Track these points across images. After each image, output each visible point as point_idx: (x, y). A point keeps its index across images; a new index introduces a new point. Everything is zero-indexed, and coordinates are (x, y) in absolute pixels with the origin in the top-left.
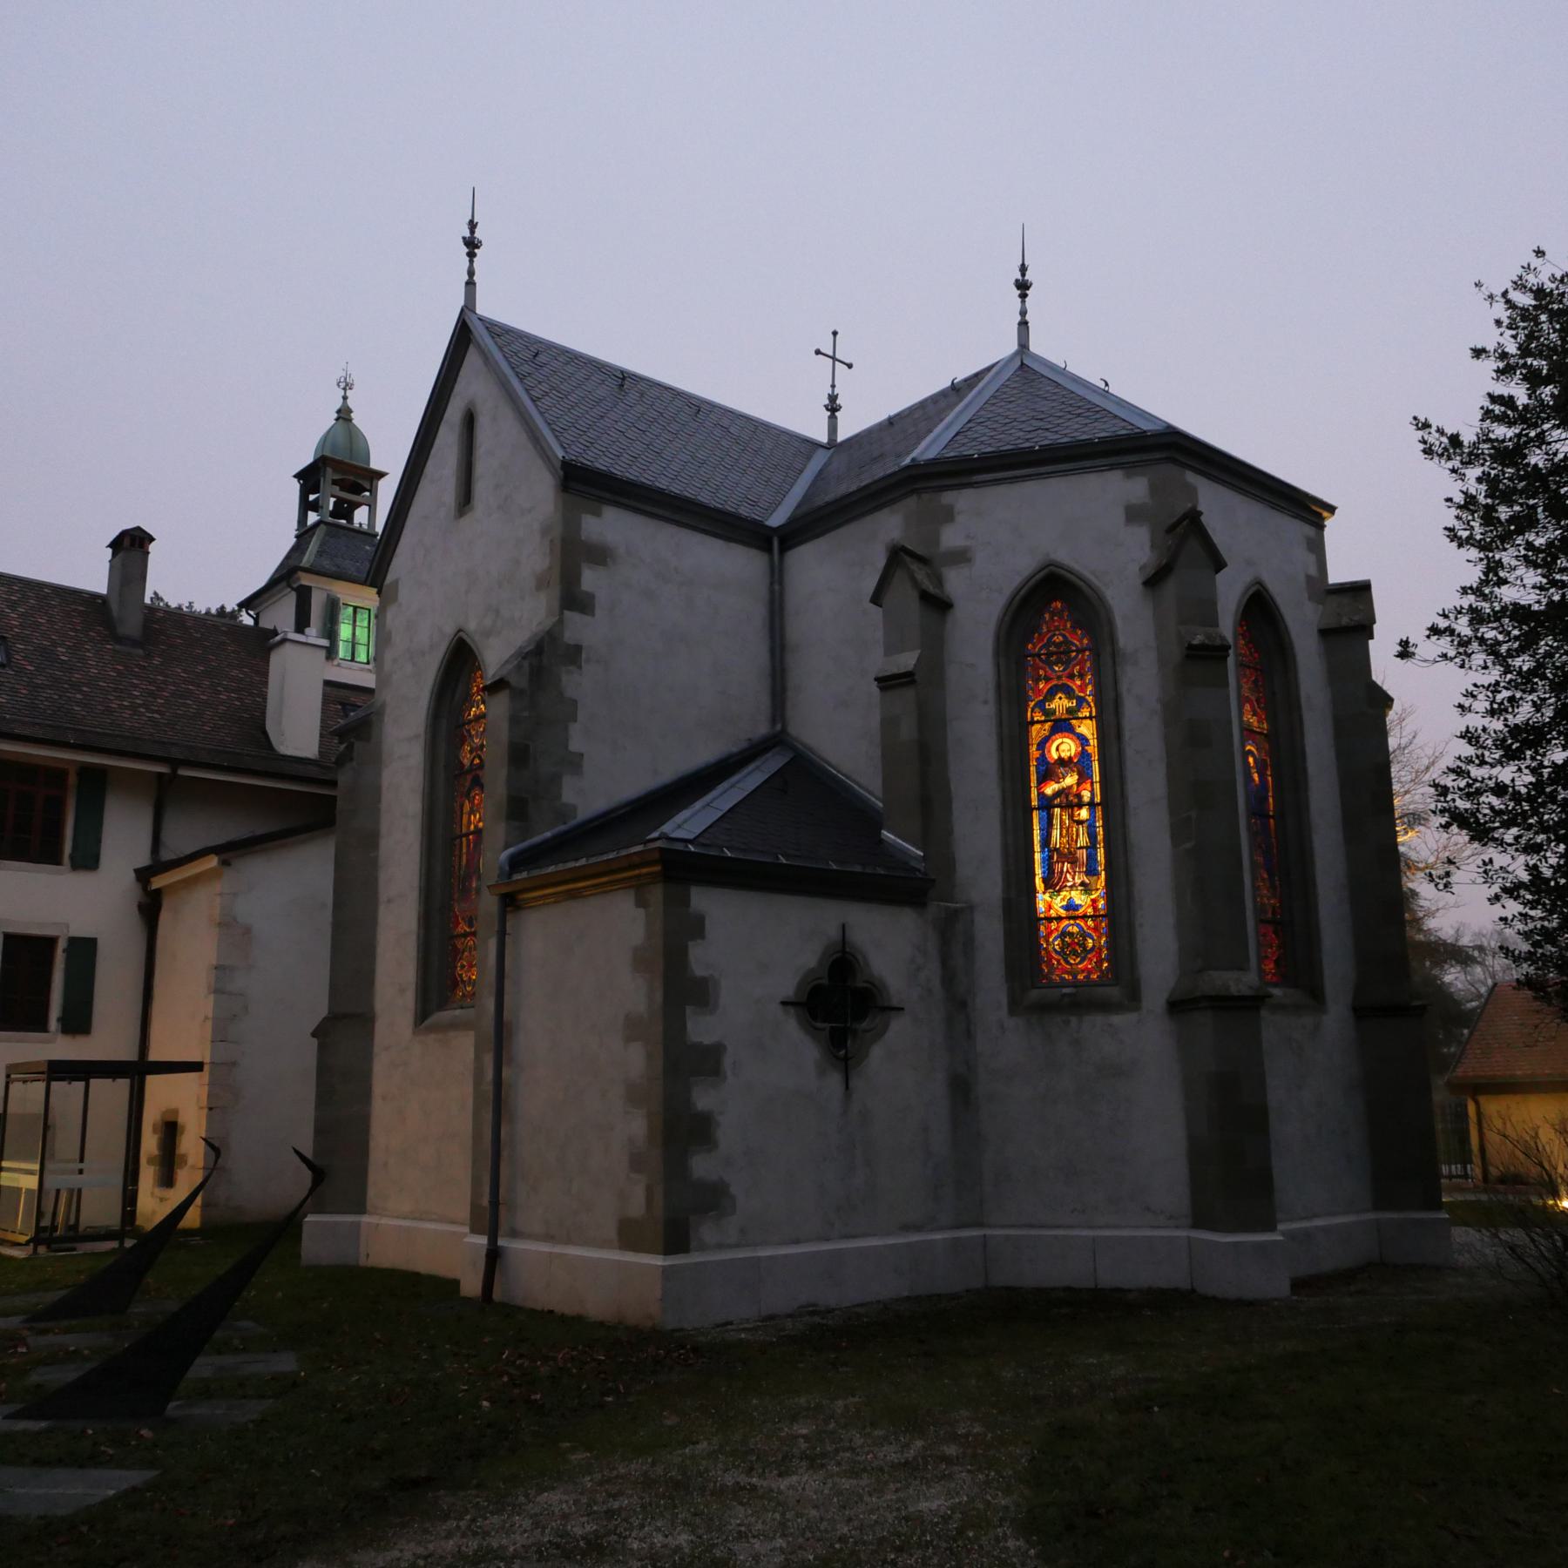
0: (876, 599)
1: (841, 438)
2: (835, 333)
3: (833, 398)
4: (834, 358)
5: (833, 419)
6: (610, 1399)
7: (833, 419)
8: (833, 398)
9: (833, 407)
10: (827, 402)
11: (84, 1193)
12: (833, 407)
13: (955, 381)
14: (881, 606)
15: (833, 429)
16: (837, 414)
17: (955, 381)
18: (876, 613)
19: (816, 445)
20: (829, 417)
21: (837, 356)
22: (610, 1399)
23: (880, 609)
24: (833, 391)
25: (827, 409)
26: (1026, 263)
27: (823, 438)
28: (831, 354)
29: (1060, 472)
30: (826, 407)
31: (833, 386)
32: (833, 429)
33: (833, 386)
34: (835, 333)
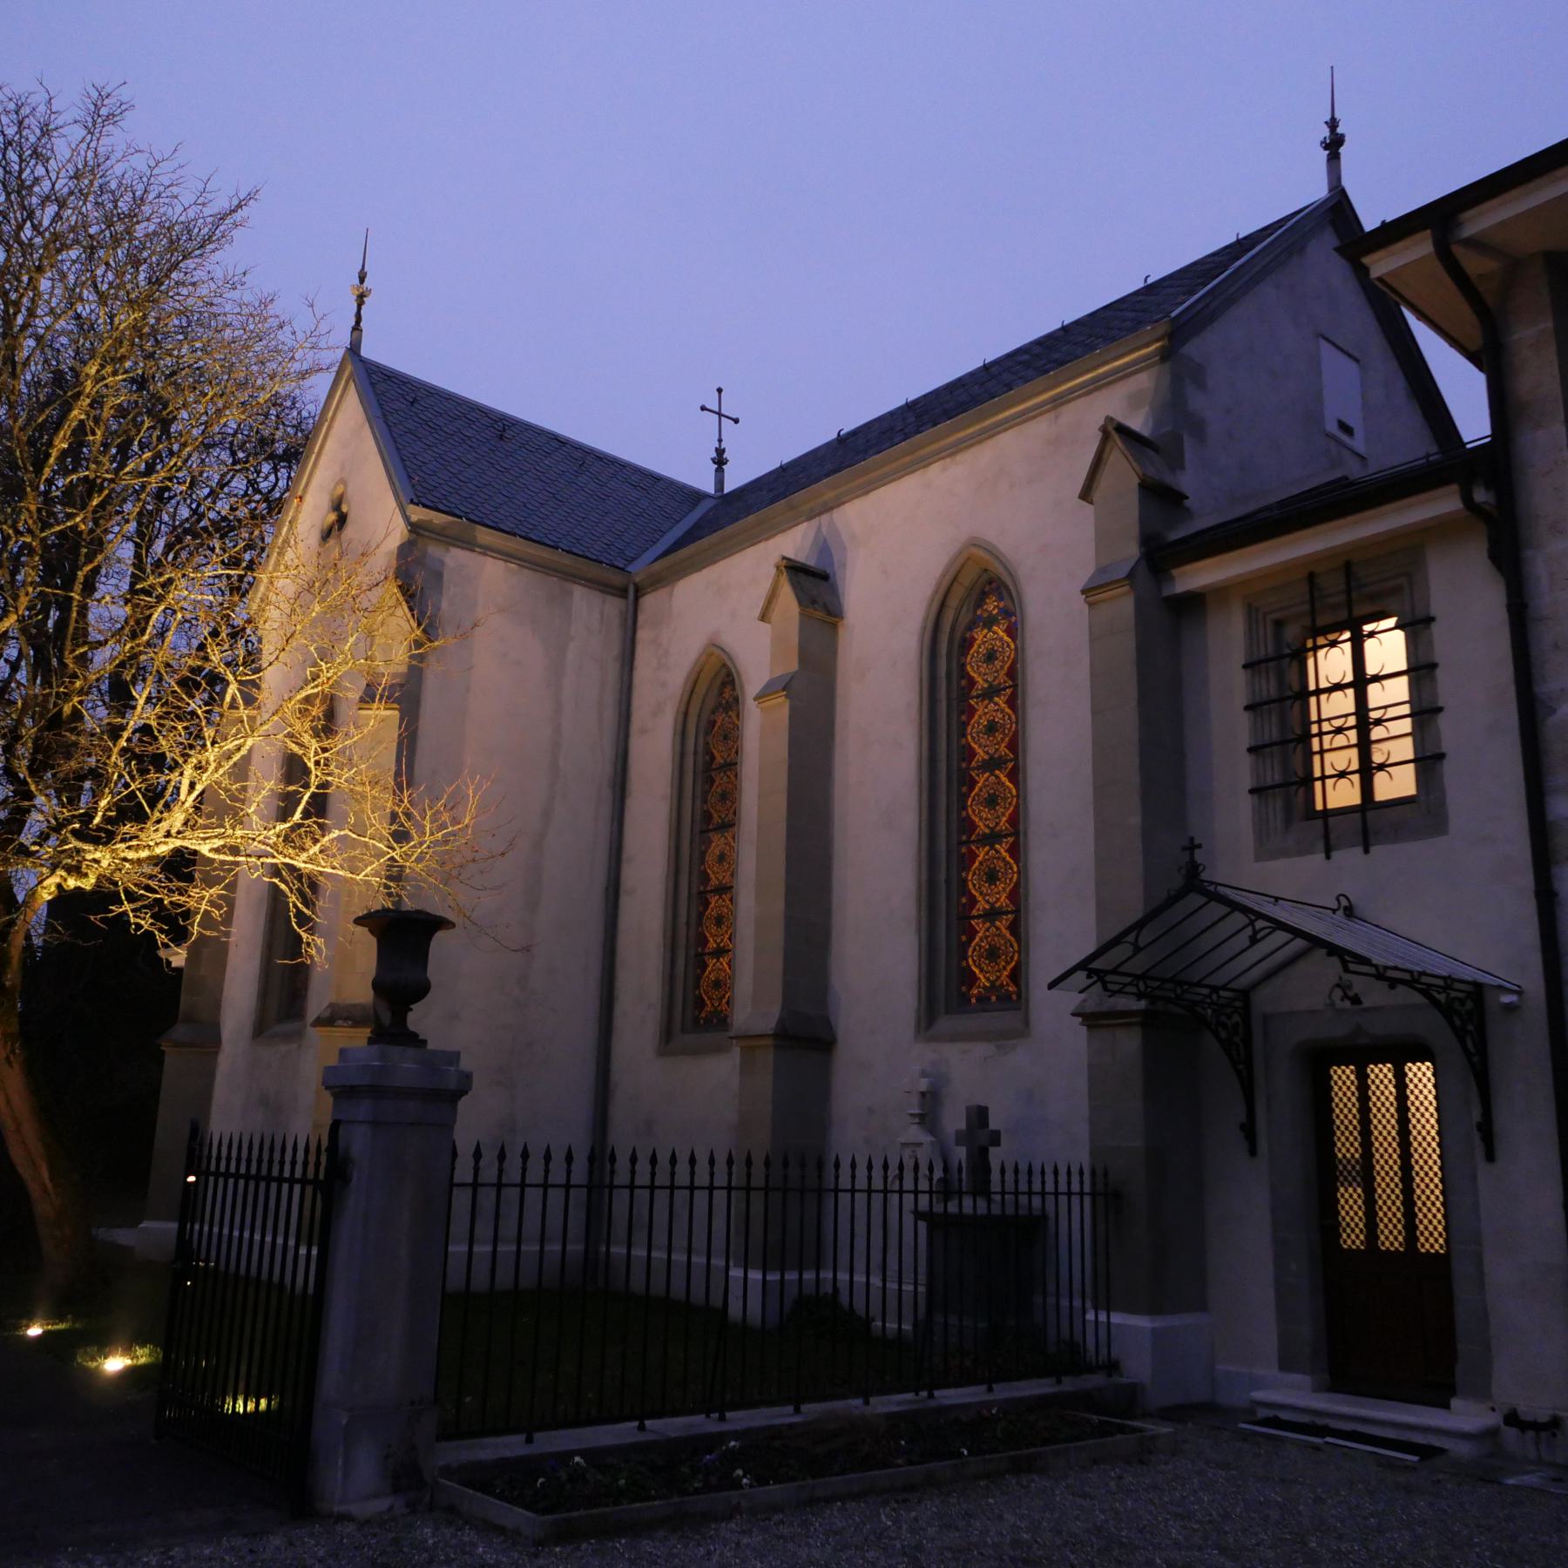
0: (1086, 494)
1: (728, 488)
2: (720, 391)
3: (720, 452)
4: (720, 414)
5: (720, 471)
6: (115, 1364)
7: (720, 471)
8: (720, 452)
9: (720, 460)
10: (715, 455)
11: (757, 612)
12: (720, 460)
13: (842, 433)
14: (1091, 503)
15: (720, 483)
16: (724, 467)
17: (842, 433)
18: (1089, 509)
19: (706, 496)
20: (717, 470)
21: (723, 412)
22: (115, 1364)
23: (1090, 506)
24: (720, 445)
25: (715, 463)
26: (1337, 116)
27: (709, 487)
28: (717, 410)
29: (1107, 584)
30: (713, 460)
31: (720, 441)
32: (720, 483)
33: (720, 441)
34: (720, 391)
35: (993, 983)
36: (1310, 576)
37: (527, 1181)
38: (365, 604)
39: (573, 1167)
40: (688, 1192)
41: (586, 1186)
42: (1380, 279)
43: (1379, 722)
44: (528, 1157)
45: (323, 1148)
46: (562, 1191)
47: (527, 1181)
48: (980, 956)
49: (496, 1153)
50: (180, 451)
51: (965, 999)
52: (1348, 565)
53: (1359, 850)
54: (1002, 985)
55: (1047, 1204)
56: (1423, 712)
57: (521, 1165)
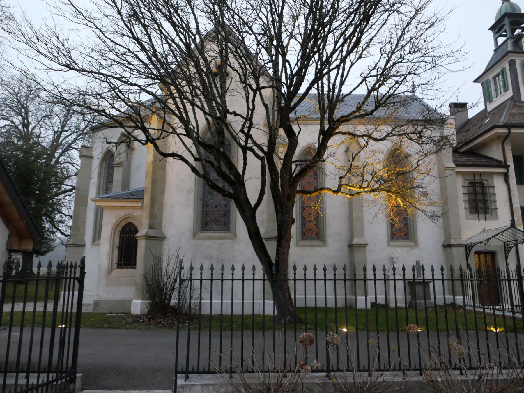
49: (220, 266)
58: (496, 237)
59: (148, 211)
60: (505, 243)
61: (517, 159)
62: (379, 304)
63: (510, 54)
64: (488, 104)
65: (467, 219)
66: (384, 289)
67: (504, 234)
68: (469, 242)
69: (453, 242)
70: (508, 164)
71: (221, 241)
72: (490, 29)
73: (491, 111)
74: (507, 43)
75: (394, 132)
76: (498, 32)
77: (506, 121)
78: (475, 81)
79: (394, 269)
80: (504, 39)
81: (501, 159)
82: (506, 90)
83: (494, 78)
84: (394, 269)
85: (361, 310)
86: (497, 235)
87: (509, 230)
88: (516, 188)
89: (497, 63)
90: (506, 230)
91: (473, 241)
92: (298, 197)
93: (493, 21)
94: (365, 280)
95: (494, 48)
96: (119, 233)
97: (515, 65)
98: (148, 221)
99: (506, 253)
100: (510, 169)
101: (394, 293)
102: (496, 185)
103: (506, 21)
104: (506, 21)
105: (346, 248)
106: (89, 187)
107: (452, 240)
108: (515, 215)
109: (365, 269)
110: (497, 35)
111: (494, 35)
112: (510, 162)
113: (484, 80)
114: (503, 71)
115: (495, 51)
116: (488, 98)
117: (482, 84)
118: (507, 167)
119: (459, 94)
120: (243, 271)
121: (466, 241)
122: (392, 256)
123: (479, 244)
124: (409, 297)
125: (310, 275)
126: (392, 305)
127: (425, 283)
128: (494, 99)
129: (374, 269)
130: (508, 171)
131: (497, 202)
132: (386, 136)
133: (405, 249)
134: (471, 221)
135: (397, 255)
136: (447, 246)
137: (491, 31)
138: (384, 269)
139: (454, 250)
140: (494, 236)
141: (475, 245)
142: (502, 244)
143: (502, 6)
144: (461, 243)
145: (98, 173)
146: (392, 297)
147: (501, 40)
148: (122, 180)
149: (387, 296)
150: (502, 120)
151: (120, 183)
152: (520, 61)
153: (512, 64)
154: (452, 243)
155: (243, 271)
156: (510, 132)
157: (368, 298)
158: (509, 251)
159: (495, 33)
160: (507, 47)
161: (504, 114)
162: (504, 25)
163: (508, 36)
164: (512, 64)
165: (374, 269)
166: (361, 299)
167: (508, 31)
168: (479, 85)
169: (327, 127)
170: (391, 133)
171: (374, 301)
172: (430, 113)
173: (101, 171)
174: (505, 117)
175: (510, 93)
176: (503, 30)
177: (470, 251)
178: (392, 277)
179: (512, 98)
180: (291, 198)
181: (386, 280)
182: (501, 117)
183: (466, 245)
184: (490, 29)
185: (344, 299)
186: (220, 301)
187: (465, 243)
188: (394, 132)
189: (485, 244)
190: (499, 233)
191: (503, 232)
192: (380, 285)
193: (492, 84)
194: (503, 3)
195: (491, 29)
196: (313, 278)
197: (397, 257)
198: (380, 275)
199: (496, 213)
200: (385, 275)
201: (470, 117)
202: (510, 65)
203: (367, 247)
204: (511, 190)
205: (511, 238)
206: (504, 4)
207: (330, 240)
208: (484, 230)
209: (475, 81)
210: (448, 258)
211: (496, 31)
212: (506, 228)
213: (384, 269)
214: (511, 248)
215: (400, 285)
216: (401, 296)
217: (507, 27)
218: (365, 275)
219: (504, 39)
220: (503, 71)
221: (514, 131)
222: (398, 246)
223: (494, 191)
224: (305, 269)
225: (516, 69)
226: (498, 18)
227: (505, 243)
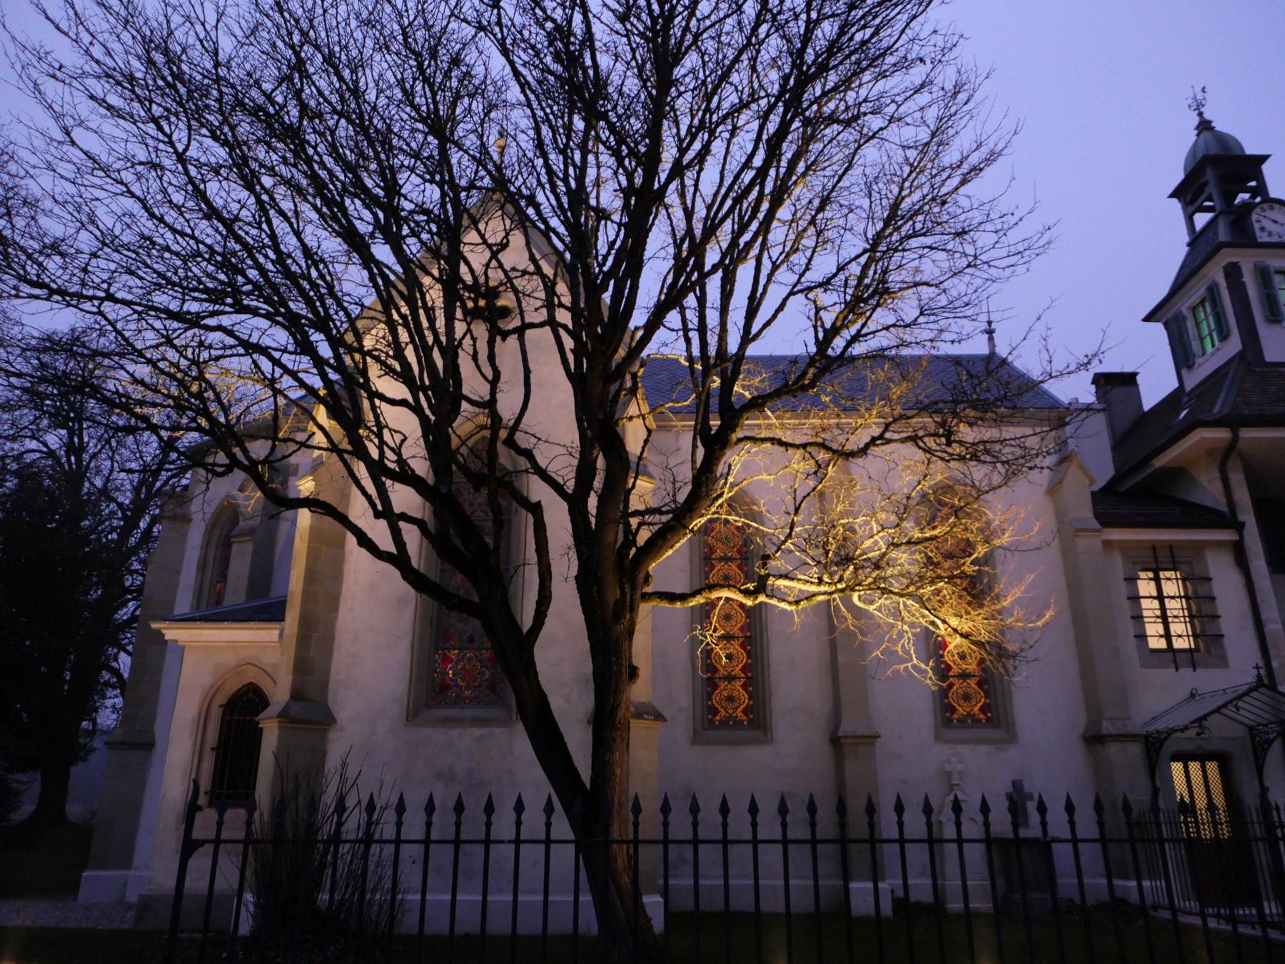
35: (968, 713)
36: (1154, 547)
37: (463, 837)
38: (149, 356)
39: (1076, 818)
40: (542, 847)
41: (1079, 841)
42: (217, 453)
43: (1158, 617)
44: (404, 810)
45: (202, 790)
46: (807, 849)
47: (463, 837)
48: (957, 698)
49: (688, 804)
50: (449, 186)
51: (950, 720)
52: (1171, 547)
53: (1192, 669)
54: (974, 715)
55: (404, 867)
56: (1138, 618)
57: (809, 820)
58: (1224, 710)
59: (293, 654)
60: (1251, 728)
61: (1260, 507)
62: (917, 904)
63: (1224, 251)
64: (1184, 372)
65: (1143, 665)
66: (927, 861)
67: (1240, 704)
68: (1151, 728)
69: (1107, 727)
70: (1241, 518)
71: (478, 732)
72: (1172, 196)
73: (1193, 390)
74: (1217, 227)
75: (888, 435)
76: (1192, 202)
77: (1226, 411)
78: (1148, 319)
79: (957, 807)
80: (1207, 217)
81: (1222, 505)
82: (1224, 337)
83: (1194, 309)
84: (957, 807)
85: (863, 920)
86: (1224, 706)
87: (1255, 694)
88: (1269, 583)
89: (1195, 272)
90: (1247, 693)
91: (1161, 725)
92: (645, 609)
93: (1179, 176)
94: (1103, 840)
95: (1186, 239)
96: (221, 710)
97: (1242, 276)
98: (290, 677)
99: (1256, 758)
100: (1246, 531)
101: (958, 871)
102: (1213, 573)
103: (1210, 175)
104: (1210, 175)
105: (826, 750)
106: (175, 594)
107: (1106, 724)
108: (1272, 652)
109: (871, 809)
110: (1191, 208)
111: (1185, 208)
112: (1248, 517)
113: (1169, 315)
114: (1213, 291)
115: (1189, 245)
116: (1183, 357)
117: (1166, 325)
118: (1239, 527)
119: (1049, 333)
120: (784, 818)
121: (1146, 724)
122: (947, 767)
123: (1179, 735)
124: (1000, 882)
125: (739, 826)
126: (955, 905)
127: (1044, 845)
128: (1199, 360)
129: (899, 808)
130: (1242, 538)
131: (1220, 620)
132: (867, 446)
133: (983, 748)
134: (1153, 671)
135: (960, 767)
136: (1094, 739)
137: (1175, 200)
138: (928, 809)
139: (1113, 749)
140: (1217, 710)
141: (1170, 735)
142: (1241, 732)
143: (1196, 142)
144: (1131, 730)
145: (199, 560)
146: (952, 883)
147: (1201, 219)
148: (251, 575)
149: (939, 881)
150: (1216, 409)
151: (244, 582)
152: (1252, 266)
153: (1233, 272)
154: (1105, 732)
155: (784, 818)
156: (1236, 439)
157: (881, 885)
158: (1265, 751)
159: (1186, 205)
160: (1216, 234)
161: (1223, 395)
162: (1206, 184)
163: (1218, 209)
164: (1233, 272)
165: (899, 808)
166: (860, 888)
167: (1215, 196)
168: (1158, 329)
169: (715, 423)
170: (881, 437)
171: (900, 893)
172: (976, 382)
173: (206, 554)
174: (1224, 402)
175: (1234, 345)
176: (1202, 198)
177: (1158, 752)
178: (950, 832)
179: (1240, 356)
180: (626, 609)
181: (933, 841)
182: (1214, 403)
183: (1147, 737)
184: (1172, 196)
185: (812, 891)
186: (511, 898)
187: (1143, 732)
188: (888, 435)
189: (1198, 734)
190: (1230, 702)
191: (1239, 698)
192: (918, 855)
193: (1190, 324)
194: (1198, 135)
195: (1173, 195)
196: (690, 836)
197: (961, 772)
198: (915, 824)
199: (1222, 647)
200: (929, 825)
201: (1147, 405)
202: (1227, 276)
203: (879, 743)
204: (1256, 586)
205: (1266, 716)
206: (1202, 135)
207: (781, 726)
208: (1192, 696)
209: (1148, 319)
210: (1100, 772)
211: (1188, 199)
212: (1245, 688)
213: (928, 809)
214: (1270, 742)
215: (975, 853)
216: (978, 880)
217: (1212, 189)
218: (872, 826)
219: (1207, 217)
220: (1213, 291)
221: (1247, 434)
222: (964, 742)
223: (1211, 589)
224: (724, 809)
225: (1243, 284)
226: (1189, 169)
227: (1251, 728)
